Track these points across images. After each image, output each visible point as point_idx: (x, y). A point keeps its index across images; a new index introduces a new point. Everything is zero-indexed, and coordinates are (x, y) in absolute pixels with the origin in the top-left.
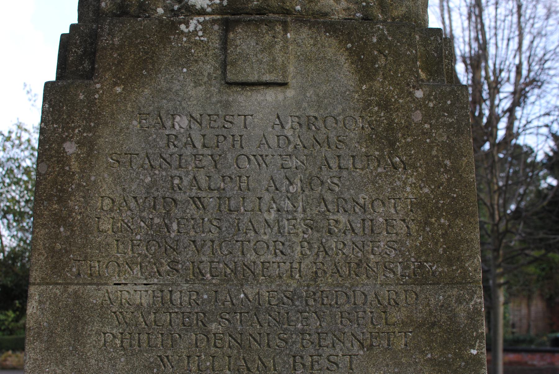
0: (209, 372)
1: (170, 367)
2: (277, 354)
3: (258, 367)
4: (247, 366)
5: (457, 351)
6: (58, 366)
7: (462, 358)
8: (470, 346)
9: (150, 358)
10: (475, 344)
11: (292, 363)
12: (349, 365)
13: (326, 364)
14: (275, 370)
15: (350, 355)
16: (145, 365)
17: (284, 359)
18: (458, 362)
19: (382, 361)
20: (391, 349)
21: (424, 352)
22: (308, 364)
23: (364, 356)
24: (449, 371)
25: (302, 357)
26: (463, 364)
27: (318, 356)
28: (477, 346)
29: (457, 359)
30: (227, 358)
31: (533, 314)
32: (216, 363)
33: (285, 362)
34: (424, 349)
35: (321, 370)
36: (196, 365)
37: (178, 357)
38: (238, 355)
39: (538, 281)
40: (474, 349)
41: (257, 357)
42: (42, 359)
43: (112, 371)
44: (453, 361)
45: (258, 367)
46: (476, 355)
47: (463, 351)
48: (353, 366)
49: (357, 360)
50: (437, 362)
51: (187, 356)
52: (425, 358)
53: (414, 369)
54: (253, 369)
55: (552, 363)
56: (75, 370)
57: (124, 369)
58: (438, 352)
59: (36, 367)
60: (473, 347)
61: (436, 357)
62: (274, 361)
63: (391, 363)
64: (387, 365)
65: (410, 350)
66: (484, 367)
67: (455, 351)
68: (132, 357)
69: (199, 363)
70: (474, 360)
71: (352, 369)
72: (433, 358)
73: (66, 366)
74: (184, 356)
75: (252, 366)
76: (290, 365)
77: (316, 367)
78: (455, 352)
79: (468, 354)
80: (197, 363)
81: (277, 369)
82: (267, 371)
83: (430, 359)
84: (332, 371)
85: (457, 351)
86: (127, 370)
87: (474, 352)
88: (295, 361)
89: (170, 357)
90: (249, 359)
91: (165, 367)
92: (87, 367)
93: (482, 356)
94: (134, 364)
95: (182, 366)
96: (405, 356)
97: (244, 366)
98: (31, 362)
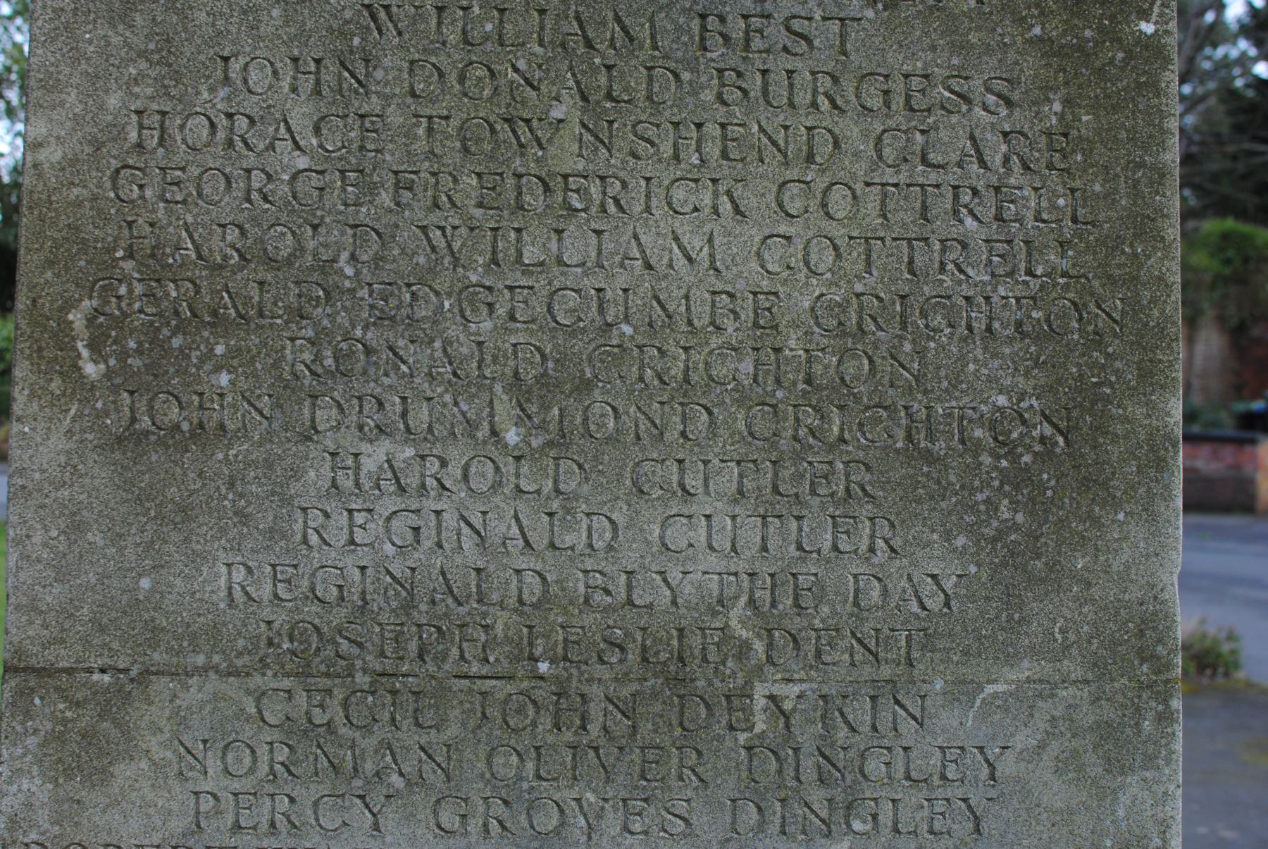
0: (489, 46)
1: (395, 33)
2: (661, 8)
3: (612, 38)
4: (585, 37)
5: (1107, 22)
6: (115, 26)
7: (1119, 40)
8: (1138, 12)
9: (343, 10)
10: (1151, 8)
11: (697, 32)
12: (837, 43)
13: (784, 38)
14: (655, 48)
15: (841, 20)
16: (331, 27)
17: (677, 22)
18: (1109, 51)
19: (920, 37)
20: (944, 9)
21: (1024, 19)
22: (737, 35)
23: (876, 22)
24: (1084, 70)
25: (722, 19)
26: (1120, 55)
27: (762, 16)
28: (1154, 14)
29: (1105, 42)
30: (536, 13)
31: (1199, 361)
32: (508, 27)
33: (679, 28)
34: (1024, 14)
35: (768, 51)
36: (459, 30)
37: (413, 10)
38: (562, 8)
39: (1213, 286)
40: (1148, 22)
41: (610, 15)
42: (76, 8)
43: (250, 41)
44: (1094, 47)
45: (612, 38)
46: (1152, 35)
47: (1121, 25)
48: (849, 47)
49: (858, 32)
50: (1055, 48)
51: (437, 8)
52: (1026, 36)
53: (1000, 61)
54: (601, 43)
55: (1236, 467)
56: (157, 38)
57: (279, 37)
58: (1060, 22)
59: (58, 28)
60: (1145, 15)
61: (1054, 33)
62: (653, 26)
63: (941, 42)
64: (933, 48)
65: (991, 13)
66: (1170, 67)
67: (1100, 23)
68: (298, 7)
69: (465, 25)
70: (1146, 47)
71: (845, 53)
72: (1046, 37)
73: (133, 26)
74: (428, 7)
75: (598, 37)
76: (692, 37)
77: (757, 43)
78: (1100, 23)
79: (1134, 32)
80: (460, 24)
81: (660, 44)
82: (634, 50)
83: (1040, 39)
84: (795, 55)
85: (1107, 22)
86: (285, 38)
87: (1148, 28)
88: (704, 28)
89: (395, 9)
90: (591, 18)
91: (380, 32)
92: (185, 29)
93: (1166, 40)
94: (305, 24)
95: (423, 32)
96: (978, 29)
97: (577, 35)
98: (47, 17)
